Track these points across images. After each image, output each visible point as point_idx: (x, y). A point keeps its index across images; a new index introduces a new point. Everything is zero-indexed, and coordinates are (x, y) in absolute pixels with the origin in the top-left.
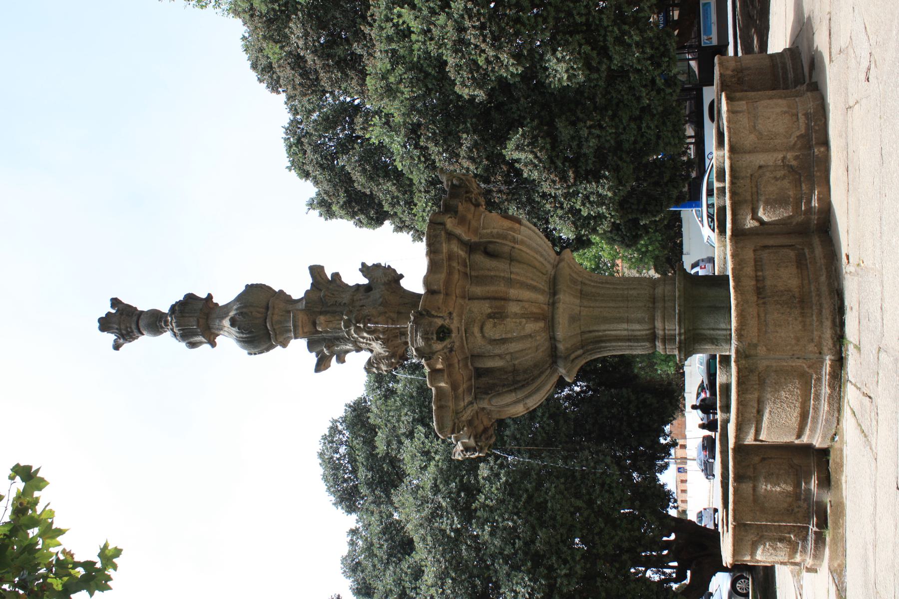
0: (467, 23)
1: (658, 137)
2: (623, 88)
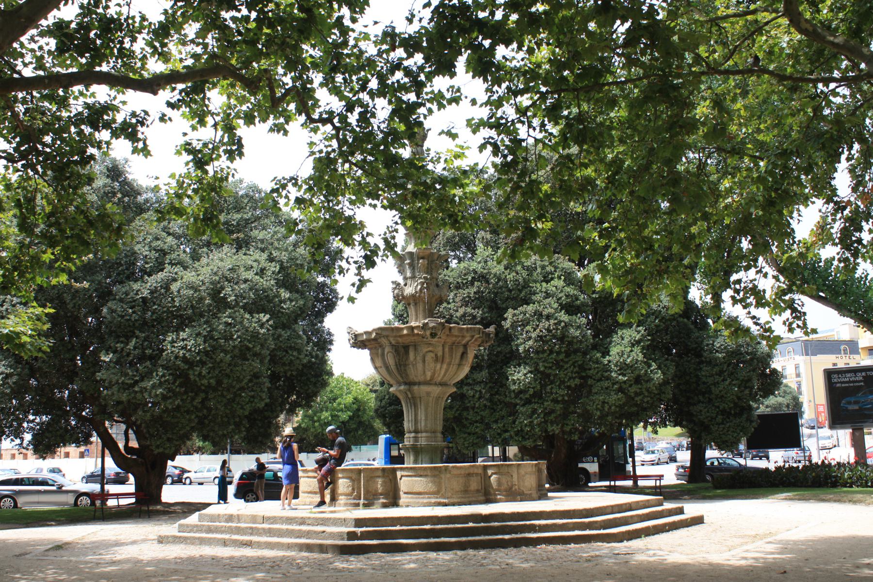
0: (552, 322)
1: (469, 434)
2: (503, 413)
